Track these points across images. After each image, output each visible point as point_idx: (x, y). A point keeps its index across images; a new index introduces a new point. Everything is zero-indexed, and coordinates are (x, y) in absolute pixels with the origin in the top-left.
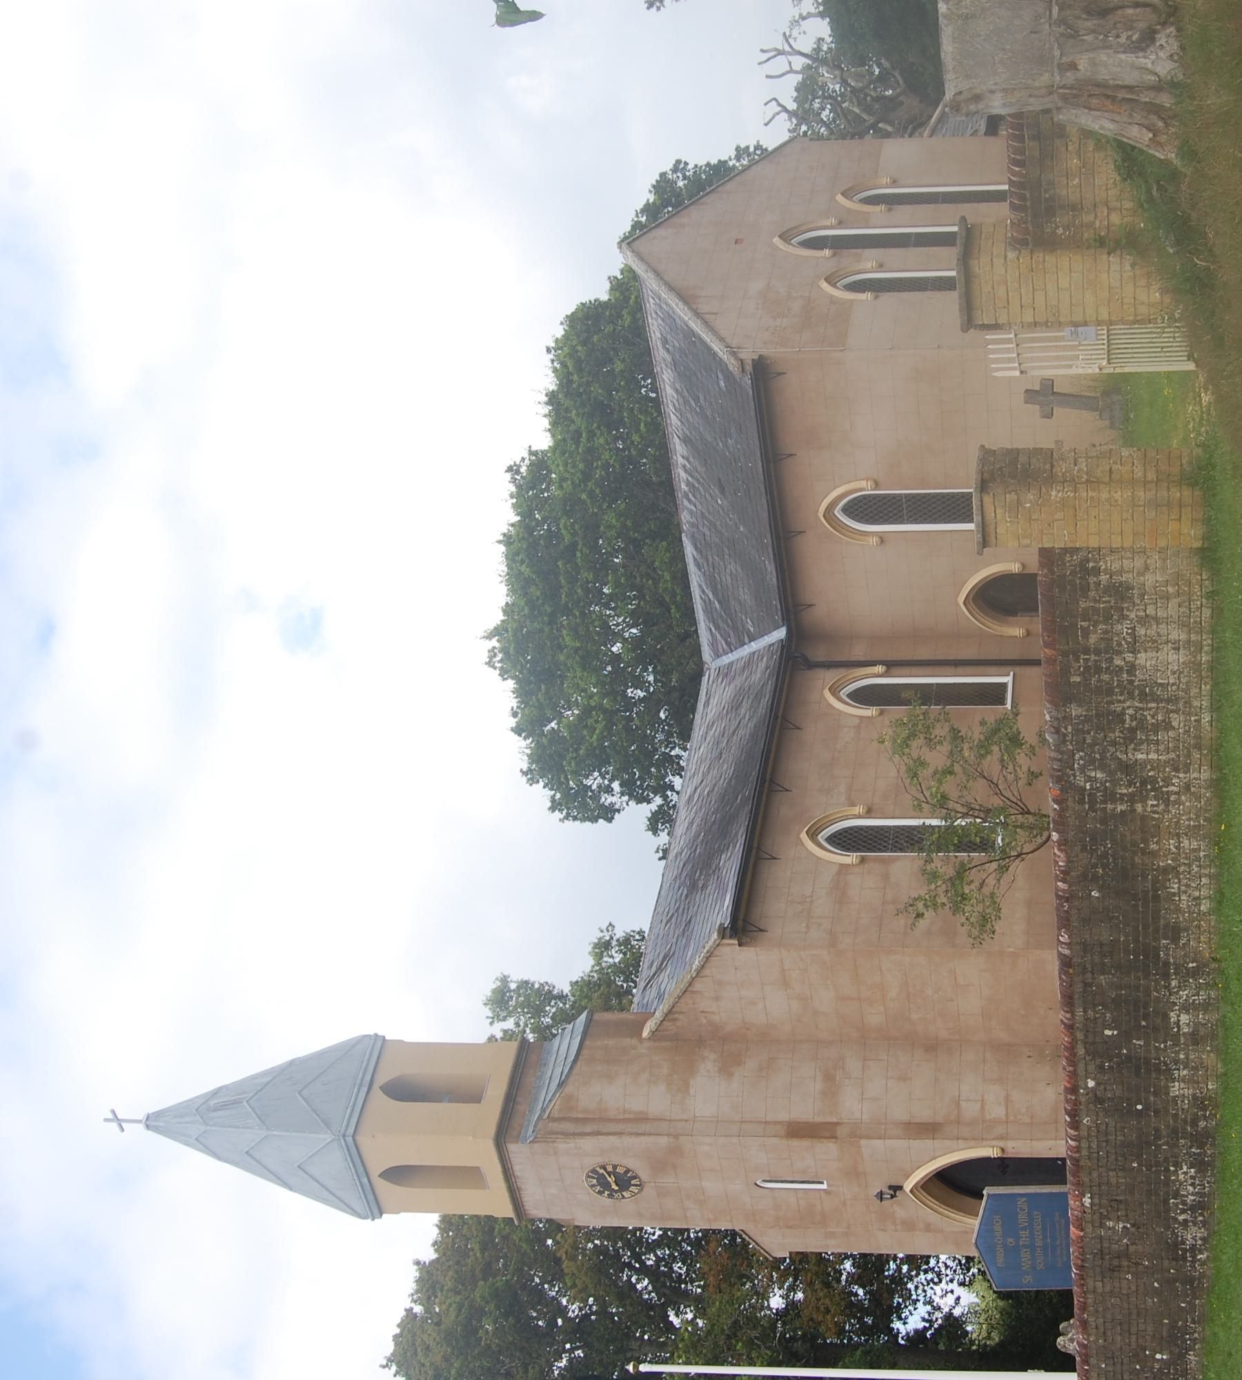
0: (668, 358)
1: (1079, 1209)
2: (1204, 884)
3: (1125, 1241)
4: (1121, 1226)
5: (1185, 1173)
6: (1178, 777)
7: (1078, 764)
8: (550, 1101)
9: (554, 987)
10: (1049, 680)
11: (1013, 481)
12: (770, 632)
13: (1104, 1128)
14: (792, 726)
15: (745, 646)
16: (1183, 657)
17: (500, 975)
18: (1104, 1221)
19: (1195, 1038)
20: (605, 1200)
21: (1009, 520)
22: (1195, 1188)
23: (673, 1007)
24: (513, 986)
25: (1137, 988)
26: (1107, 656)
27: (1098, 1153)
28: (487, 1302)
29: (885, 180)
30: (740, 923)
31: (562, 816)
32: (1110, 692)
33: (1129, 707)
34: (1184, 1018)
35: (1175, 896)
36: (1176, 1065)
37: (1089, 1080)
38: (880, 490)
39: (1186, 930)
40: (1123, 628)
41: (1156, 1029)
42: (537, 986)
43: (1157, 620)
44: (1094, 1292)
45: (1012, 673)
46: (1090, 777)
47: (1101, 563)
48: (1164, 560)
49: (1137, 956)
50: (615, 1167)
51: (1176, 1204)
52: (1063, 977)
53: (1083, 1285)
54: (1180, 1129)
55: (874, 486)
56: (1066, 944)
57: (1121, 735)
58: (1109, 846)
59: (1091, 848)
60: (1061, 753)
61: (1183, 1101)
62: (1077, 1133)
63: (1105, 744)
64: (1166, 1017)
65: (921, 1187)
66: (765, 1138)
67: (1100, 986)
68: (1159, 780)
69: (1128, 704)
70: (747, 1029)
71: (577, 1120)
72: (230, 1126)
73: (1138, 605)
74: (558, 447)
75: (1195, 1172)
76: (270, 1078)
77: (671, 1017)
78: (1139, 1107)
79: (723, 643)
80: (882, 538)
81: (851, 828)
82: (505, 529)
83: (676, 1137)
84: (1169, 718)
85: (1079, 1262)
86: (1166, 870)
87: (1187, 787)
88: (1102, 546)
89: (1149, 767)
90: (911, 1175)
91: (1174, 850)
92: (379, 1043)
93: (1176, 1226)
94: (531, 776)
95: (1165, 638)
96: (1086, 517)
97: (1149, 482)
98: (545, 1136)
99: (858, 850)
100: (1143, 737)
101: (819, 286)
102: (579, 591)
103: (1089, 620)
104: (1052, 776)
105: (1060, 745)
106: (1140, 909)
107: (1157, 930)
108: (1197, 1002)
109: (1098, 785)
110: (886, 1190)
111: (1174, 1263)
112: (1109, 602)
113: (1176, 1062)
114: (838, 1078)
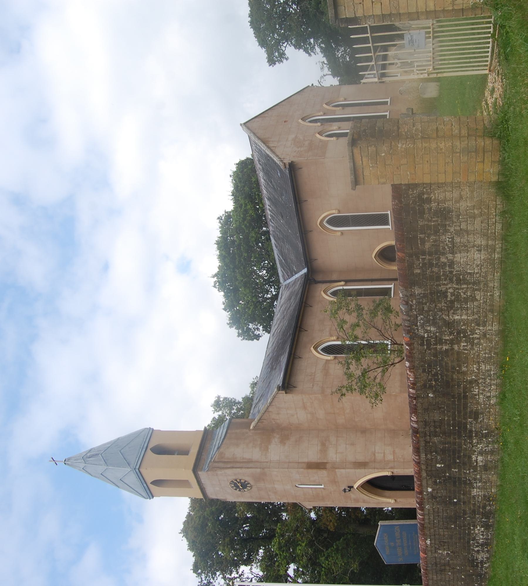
0: (261, 168)
1: (424, 545)
2: (493, 389)
3: (448, 559)
4: (445, 552)
5: (479, 530)
6: (479, 329)
7: (420, 322)
8: (214, 455)
9: (236, 400)
10: (401, 272)
11: (373, 139)
12: (302, 270)
13: (437, 510)
14: (308, 306)
15: (294, 276)
16: (483, 255)
17: (217, 396)
18: (437, 550)
19: (486, 468)
20: (237, 492)
21: (371, 165)
22: (483, 536)
23: (261, 417)
24: (221, 399)
25: (455, 443)
26: (436, 256)
27: (434, 521)
28: (210, 516)
29: (342, 99)
30: (286, 385)
31: (242, 339)
32: (438, 278)
33: (450, 288)
34: (480, 458)
35: (476, 396)
36: (475, 481)
37: (429, 488)
38: (340, 214)
39: (482, 413)
40: (446, 238)
41: (465, 464)
42: (230, 399)
43: (467, 232)
44: (432, 580)
45: (393, 284)
46: (427, 330)
47: (432, 195)
48: (472, 192)
49: (454, 427)
50: (240, 480)
51: (474, 544)
52: (414, 438)
53: (427, 577)
54: (476, 510)
55: (338, 212)
56: (415, 421)
57: (445, 305)
58: (439, 369)
59: (428, 370)
60: (410, 316)
61: (478, 498)
62: (423, 512)
63: (436, 310)
64: (470, 457)
65: (361, 487)
66: (298, 469)
67: (434, 443)
68: (468, 331)
69: (449, 286)
70: (291, 425)
71: (225, 462)
72: (94, 464)
73: (456, 222)
74: (235, 210)
75: (484, 529)
76: (110, 445)
77: (261, 421)
78: (455, 500)
79: (287, 275)
80: (342, 233)
81: (331, 345)
82: (217, 239)
83: (263, 469)
84: (474, 294)
85: (425, 568)
86: (471, 382)
87: (485, 335)
88: (433, 182)
89: (462, 324)
90: (356, 482)
91: (476, 370)
92: (151, 431)
93: (474, 552)
94: (231, 325)
95: (473, 244)
96: (421, 162)
97: (463, 137)
98: (212, 469)
99: (334, 354)
100: (459, 306)
101: (316, 136)
102: (242, 260)
103: (425, 233)
104: (404, 330)
105: (409, 311)
106: (456, 403)
107: (465, 414)
108: (487, 450)
109: (432, 335)
110: (347, 488)
111: (472, 568)
112: (437, 221)
113: (475, 479)
114: (327, 445)
